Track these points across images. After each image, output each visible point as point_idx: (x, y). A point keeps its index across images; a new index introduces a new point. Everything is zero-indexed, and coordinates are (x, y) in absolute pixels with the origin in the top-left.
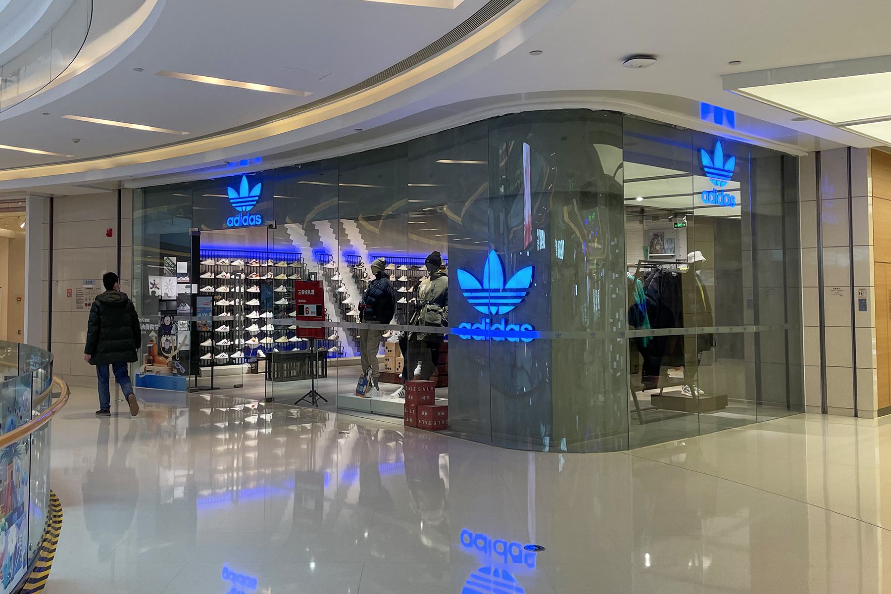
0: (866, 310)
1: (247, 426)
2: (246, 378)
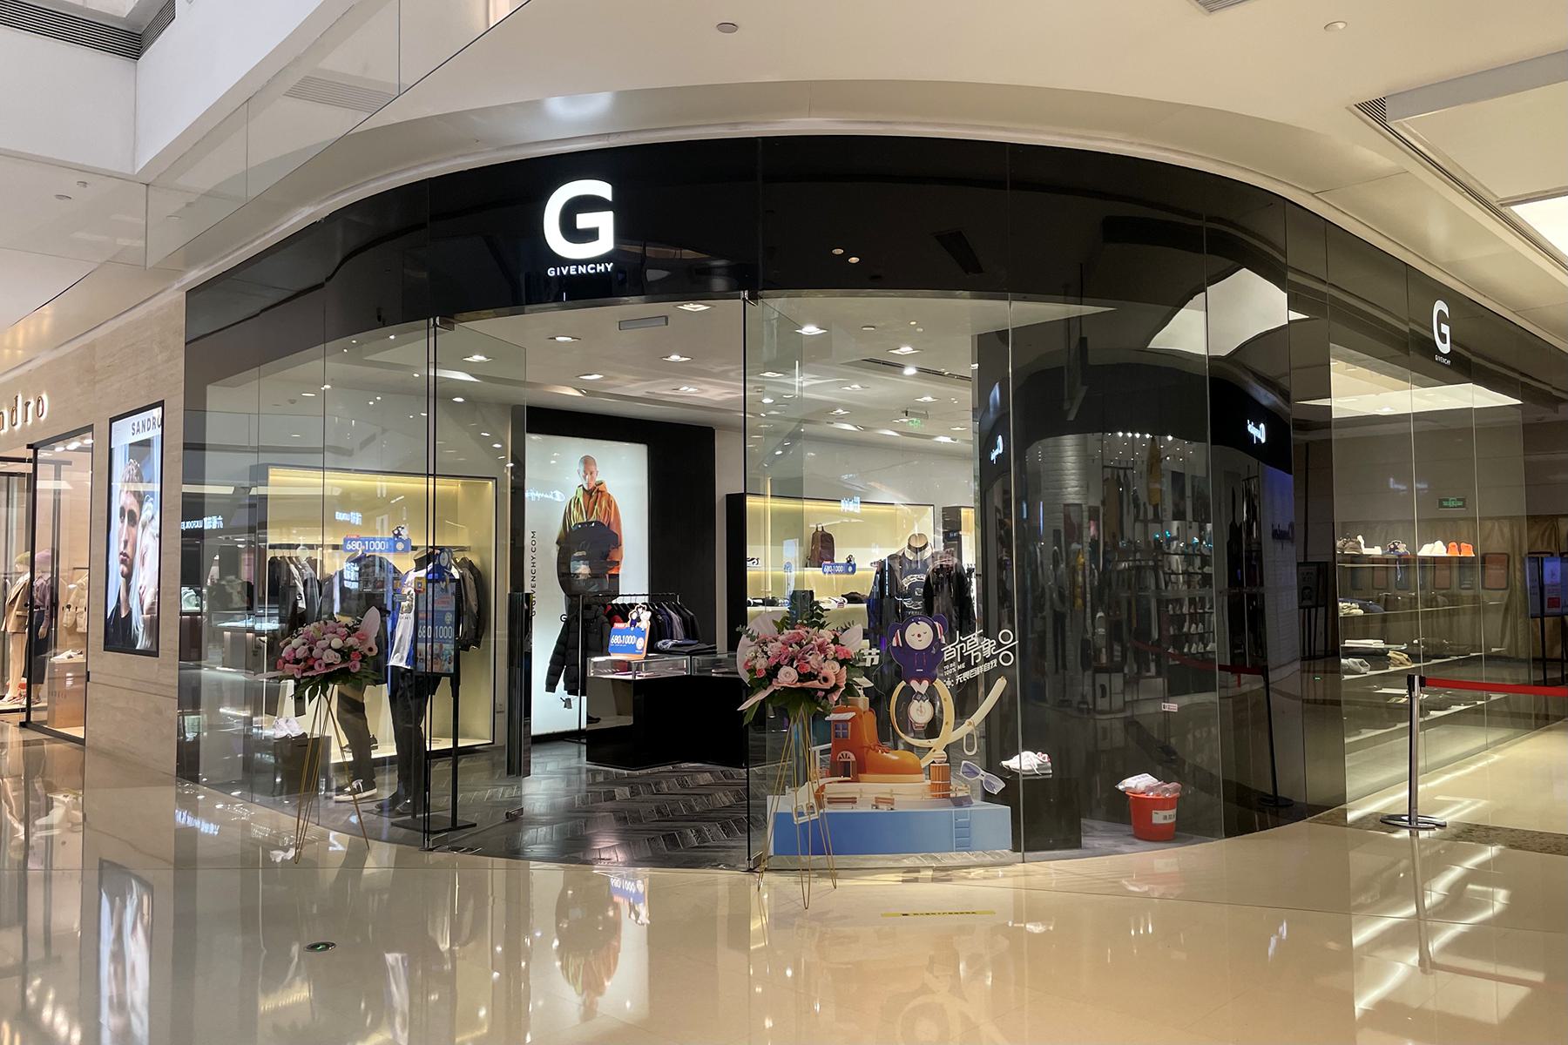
0: (104, 650)
1: (439, 555)
2: (919, 704)
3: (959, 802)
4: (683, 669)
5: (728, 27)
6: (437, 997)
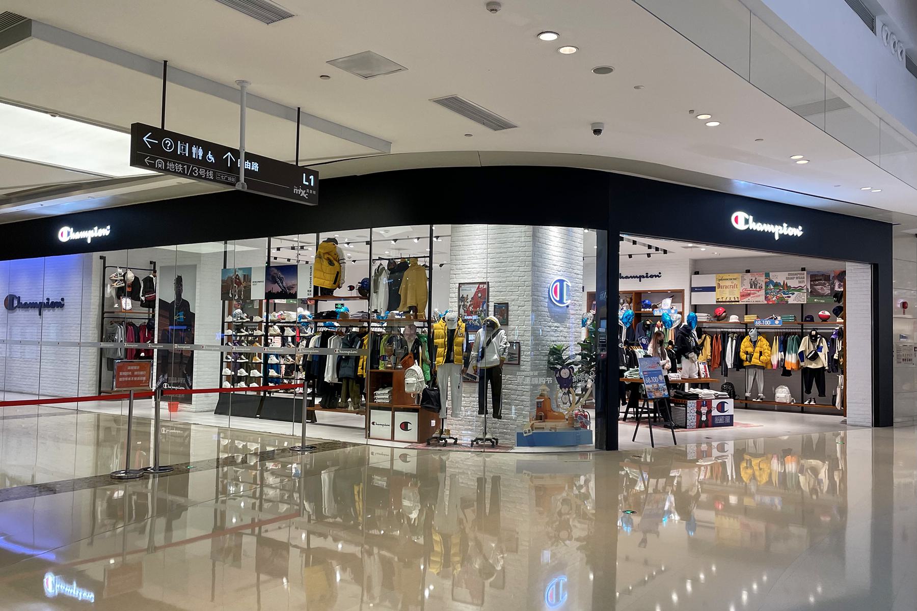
3: (577, 429)
4: (475, 390)
5: (603, 70)
6: (901, 465)
